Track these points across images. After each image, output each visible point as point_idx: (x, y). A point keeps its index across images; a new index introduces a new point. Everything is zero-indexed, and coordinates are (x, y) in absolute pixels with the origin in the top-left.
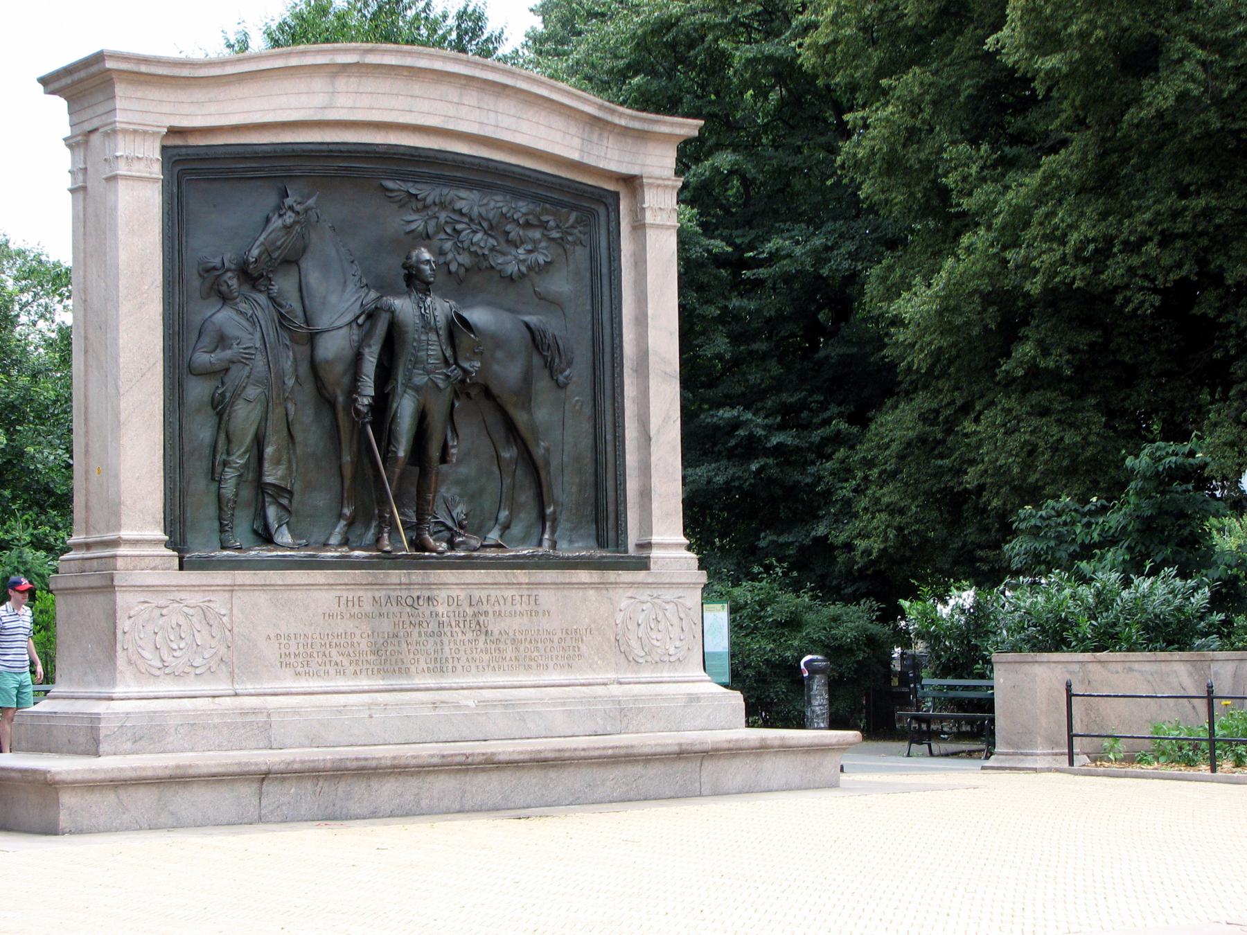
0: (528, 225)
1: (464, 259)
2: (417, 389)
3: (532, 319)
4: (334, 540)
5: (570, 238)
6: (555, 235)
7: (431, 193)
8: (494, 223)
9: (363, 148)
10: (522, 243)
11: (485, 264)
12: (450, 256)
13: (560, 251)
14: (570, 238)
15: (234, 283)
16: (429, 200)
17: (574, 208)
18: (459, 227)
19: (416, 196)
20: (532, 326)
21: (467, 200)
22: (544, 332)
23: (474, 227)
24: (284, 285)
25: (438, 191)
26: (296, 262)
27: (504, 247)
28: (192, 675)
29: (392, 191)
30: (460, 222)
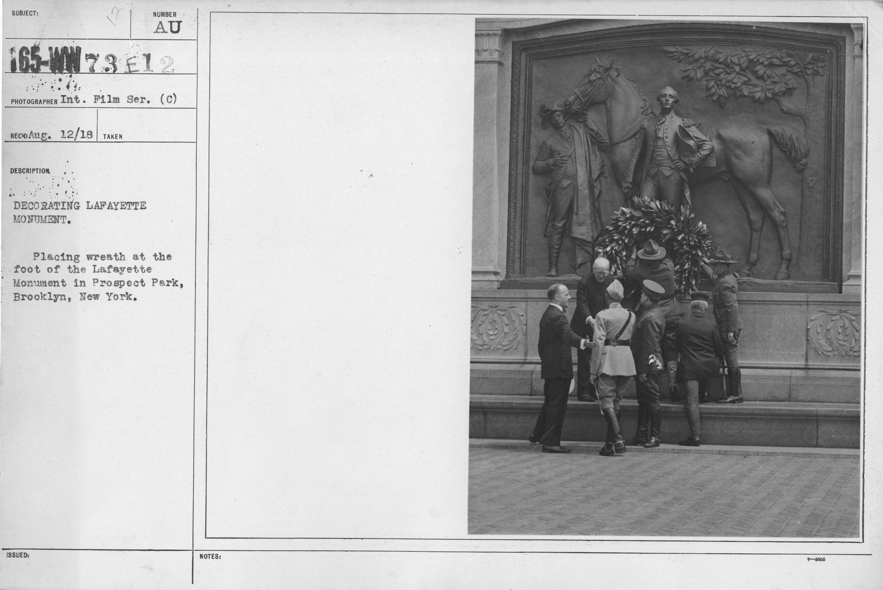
0: (771, 65)
1: (723, 91)
2: (653, 177)
3: (776, 129)
4: (781, 275)
5: (809, 72)
6: (796, 70)
7: (700, 51)
8: (744, 66)
9: (649, 28)
10: (769, 77)
11: (738, 93)
12: (713, 90)
13: (802, 80)
14: (809, 72)
15: (561, 119)
16: (696, 57)
17: (811, 50)
18: (717, 71)
19: (688, 54)
20: (773, 132)
21: (725, 53)
22: (782, 135)
23: (728, 70)
24: (594, 118)
25: (704, 49)
26: (604, 102)
27: (755, 81)
28: (103, 297)
29: (672, 53)
30: (718, 68)
